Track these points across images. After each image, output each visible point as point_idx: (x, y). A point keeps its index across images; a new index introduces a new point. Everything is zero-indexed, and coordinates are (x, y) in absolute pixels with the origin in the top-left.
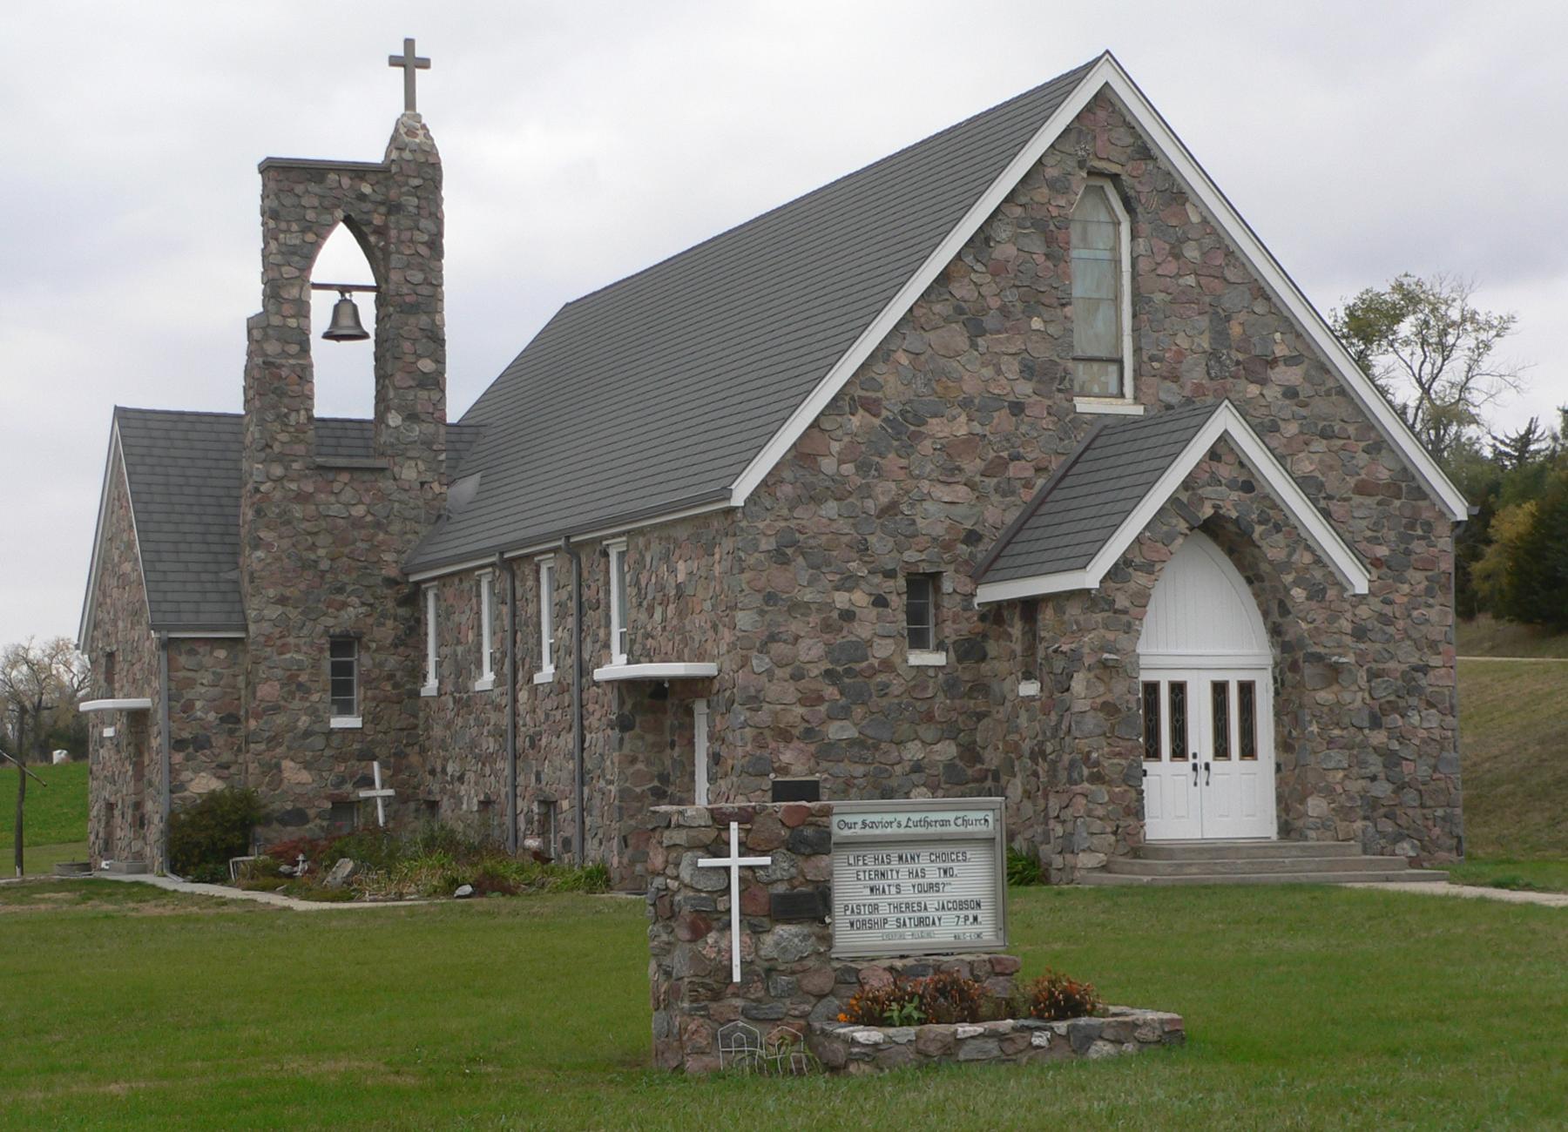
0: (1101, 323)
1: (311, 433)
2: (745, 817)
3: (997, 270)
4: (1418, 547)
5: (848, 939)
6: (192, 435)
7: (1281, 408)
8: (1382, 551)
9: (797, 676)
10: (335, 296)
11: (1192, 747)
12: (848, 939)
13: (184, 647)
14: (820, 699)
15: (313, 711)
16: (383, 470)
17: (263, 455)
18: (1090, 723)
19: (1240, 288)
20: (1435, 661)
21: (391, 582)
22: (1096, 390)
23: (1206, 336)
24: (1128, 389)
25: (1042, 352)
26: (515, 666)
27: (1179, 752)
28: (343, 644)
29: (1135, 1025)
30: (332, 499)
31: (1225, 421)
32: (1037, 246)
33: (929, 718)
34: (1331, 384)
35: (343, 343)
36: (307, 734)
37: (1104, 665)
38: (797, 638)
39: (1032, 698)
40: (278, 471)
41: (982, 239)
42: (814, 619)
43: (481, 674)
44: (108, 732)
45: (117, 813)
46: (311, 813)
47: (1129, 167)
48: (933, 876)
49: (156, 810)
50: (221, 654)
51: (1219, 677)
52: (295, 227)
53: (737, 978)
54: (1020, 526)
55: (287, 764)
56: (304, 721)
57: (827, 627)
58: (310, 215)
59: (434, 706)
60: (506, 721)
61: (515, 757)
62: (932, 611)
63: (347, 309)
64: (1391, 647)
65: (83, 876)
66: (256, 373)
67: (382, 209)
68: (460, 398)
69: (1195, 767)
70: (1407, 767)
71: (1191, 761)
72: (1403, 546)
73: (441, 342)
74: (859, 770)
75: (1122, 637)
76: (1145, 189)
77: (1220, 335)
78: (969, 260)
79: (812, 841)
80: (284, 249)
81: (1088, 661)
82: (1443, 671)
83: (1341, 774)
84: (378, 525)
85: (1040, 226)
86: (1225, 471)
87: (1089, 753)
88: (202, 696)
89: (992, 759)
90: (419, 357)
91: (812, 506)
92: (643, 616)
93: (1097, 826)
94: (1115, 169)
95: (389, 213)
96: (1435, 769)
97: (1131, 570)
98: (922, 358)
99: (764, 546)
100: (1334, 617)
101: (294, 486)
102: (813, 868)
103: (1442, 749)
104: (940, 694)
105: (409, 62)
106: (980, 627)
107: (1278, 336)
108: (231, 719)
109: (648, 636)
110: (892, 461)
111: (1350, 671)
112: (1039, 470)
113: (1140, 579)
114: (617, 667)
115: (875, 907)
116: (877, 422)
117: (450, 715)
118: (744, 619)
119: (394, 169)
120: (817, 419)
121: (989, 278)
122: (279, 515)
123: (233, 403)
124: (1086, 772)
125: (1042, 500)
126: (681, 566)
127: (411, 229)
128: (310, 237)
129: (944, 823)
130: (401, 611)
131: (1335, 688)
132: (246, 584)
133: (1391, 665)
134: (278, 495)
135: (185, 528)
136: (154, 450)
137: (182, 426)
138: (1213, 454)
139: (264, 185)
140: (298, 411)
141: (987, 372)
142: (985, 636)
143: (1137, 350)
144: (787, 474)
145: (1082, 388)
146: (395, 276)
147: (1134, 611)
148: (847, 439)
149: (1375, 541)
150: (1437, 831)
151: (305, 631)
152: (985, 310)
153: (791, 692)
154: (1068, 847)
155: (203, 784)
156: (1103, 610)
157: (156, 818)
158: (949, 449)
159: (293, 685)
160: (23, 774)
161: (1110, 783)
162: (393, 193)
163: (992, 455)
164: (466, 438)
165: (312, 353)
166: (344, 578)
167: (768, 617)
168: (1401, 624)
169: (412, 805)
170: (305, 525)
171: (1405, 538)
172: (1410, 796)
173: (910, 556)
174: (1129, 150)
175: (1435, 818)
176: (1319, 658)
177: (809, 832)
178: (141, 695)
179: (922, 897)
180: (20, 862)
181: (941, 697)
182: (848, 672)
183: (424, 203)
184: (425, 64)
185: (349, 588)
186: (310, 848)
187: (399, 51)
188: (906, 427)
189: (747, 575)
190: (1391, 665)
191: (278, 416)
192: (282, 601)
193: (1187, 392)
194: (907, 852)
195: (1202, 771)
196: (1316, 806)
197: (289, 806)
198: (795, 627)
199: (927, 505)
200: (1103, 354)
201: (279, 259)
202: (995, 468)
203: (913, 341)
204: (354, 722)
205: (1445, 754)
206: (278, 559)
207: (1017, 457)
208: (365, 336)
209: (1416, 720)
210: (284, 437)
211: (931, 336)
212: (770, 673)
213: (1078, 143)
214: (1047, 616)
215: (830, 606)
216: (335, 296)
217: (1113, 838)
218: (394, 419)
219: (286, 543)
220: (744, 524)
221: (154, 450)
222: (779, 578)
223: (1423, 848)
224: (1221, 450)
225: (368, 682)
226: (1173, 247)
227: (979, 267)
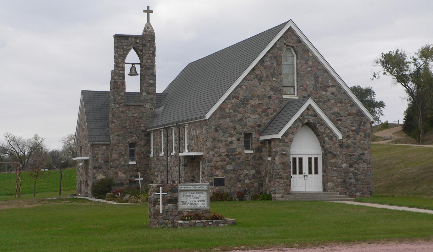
0: (290, 79)
1: (125, 97)
2: (163, 186)
3: (265, 68)
4: (362, 127)
5: (181, 206)
6: (99, 97)
8: (354, 128)
9: (220, 156)
10: (131, 66)
11: (303, 172)
12: (181, 206)
13: (96, 146)
14: (225, 161)
15: (125, 160)
16: (141, 105)
17: (114, 102)
18: (279, 166)
20: (366, 152)
21: (143, 131)
22: (288, 93)
23: (313, 81)
24: (296, 93)
25: (275, 85)
26: (168, 151)
27: (301, 172)
28: (132, 145)
29: (227, 221)
30: (130, 112)
31: (310, 102)
32: (275, 63)
33: (249, 164)
34: (342, 91)
36: (124, 166)
37: (282, 154)
38: (220, 148)
39: (270, 161)
40: (117, 106)
41: (262, 61)
42: (224, 143)
43: (161, 153)
44: (80, 164)
45: (82, 183)
46: (125, 183)
47: (296, 44)
48: (197, 196)
49: (90, 182)
50: (105, 147)
51: (310, 156)
53: (161, 212)
54: (270, 123)
55: (119, 172)
56: (123, 163)
57: (227, 145)
58: (125, 47)
59: (152, 159)
60: (166, 164)
61: (167, 171)
62: (250, 141)
63: (133, 69)
65: (74, 197)
66: (112, 84)
68: (160, 89)
69: (304, 176)
70: (359, 176)
71: (303, 174)
73: (155, 76)
74: (233, 176)
75: (286, 148)
76: (300, 49)
77: (316, 81)
78: (259, 65)
79: (174, 190)
82: (368, 155)
83: (336, 178)
84: (140, 118)
85: (275, 58)
86: (310, 112)
88: (100, 157)
89: (263, 173)
90: (150, 79)
92: (191, 142)
93: (280, 188)
94: (293, 45)
95: (143, 47)
96: (365, 176)
99: (213, 128)
100: (335, 144)
101: (121, 109)
102: (175, 195)
103: (367, 172)
104: (252, 160)
105: (148, 11)
106: (261, 145)
107: (330, 81)
108: (107, 162)
109: (191, 146)
110: (241, 109)
112: (274, 111)
113: (291, 136)
114: (186, 153)
115: (187, 201)
116: (238, 101)
117: (155, 162)
118: (208, 143)
119: (144, 36)
120: (225, 101)
122: (118, 116)
124: (278, 177)
125: (275, 117)
126: (197, 131)
128: (125, 52)
129: (199, 187)
130: (145, 138)
131: (335, 159)
132: (110, 131)
133: (356, 153)
134: (117, 111)
135: (97, 118)
136: (89, 99)
137: (97, 94)
138: (308, 109)
139: (115, 41)
141: (263, 90)
142: (262, 147)
143: (297, 85)
146: (144, 61)
147: (290, 143)
148: (231, 105)
149: (352, 126)
150: (366, 190)
151: (123, 142)
152: (262, 76)
153: (218, 159)
154: (275, 193)
155: (100, 177)
157: (90, 184)
158: (254, 106)
159: (121, 154)
160: (61, 174)
161: (284, 179)
162: (144, 42)
163: (264, 108)
164: (163, 97)
165: (125, 79)
166: (132, 130)
168: (358, 144)
169: (148, 182)
170: (124, 118)
172: (359, 182)
173: (245, 130)
176: (331, 153)
177: (174, 189)
178: (87, 156)
179: (195, 200)
180: (60, 194)
181: (252, 160)
184: (152, 12)
185: (134, 132)
186: (122, 191)
187: (146, 9)
188: (244, 102)
189: (209, 134)
190: (356, 153)
191: (117, 93)
192: (118, 135)
193: (309, 94)
194: (192, 192)
196: (330, 184)
197: (120, 182)
198: (219, 145)
199: (249, 119)
200: (290, 85)
201: (118, 57)
202: (265, 111)
203: (246, 83)
204: (134, 163)
206: (117, 126)
207: (269, 108)
208: (138, 75)
209: (361, 165)
211: (250, 82)
212: (214, 155)
214: (273, 143)
215: (227, 141)
216: (131, 66)
218: (144, 94)
219: (119, 122)
221: (89, 99)
222: (216, 135)
223: (362, 194)
224: (309, 108)
225: (138, 154)
226: (306, 62)
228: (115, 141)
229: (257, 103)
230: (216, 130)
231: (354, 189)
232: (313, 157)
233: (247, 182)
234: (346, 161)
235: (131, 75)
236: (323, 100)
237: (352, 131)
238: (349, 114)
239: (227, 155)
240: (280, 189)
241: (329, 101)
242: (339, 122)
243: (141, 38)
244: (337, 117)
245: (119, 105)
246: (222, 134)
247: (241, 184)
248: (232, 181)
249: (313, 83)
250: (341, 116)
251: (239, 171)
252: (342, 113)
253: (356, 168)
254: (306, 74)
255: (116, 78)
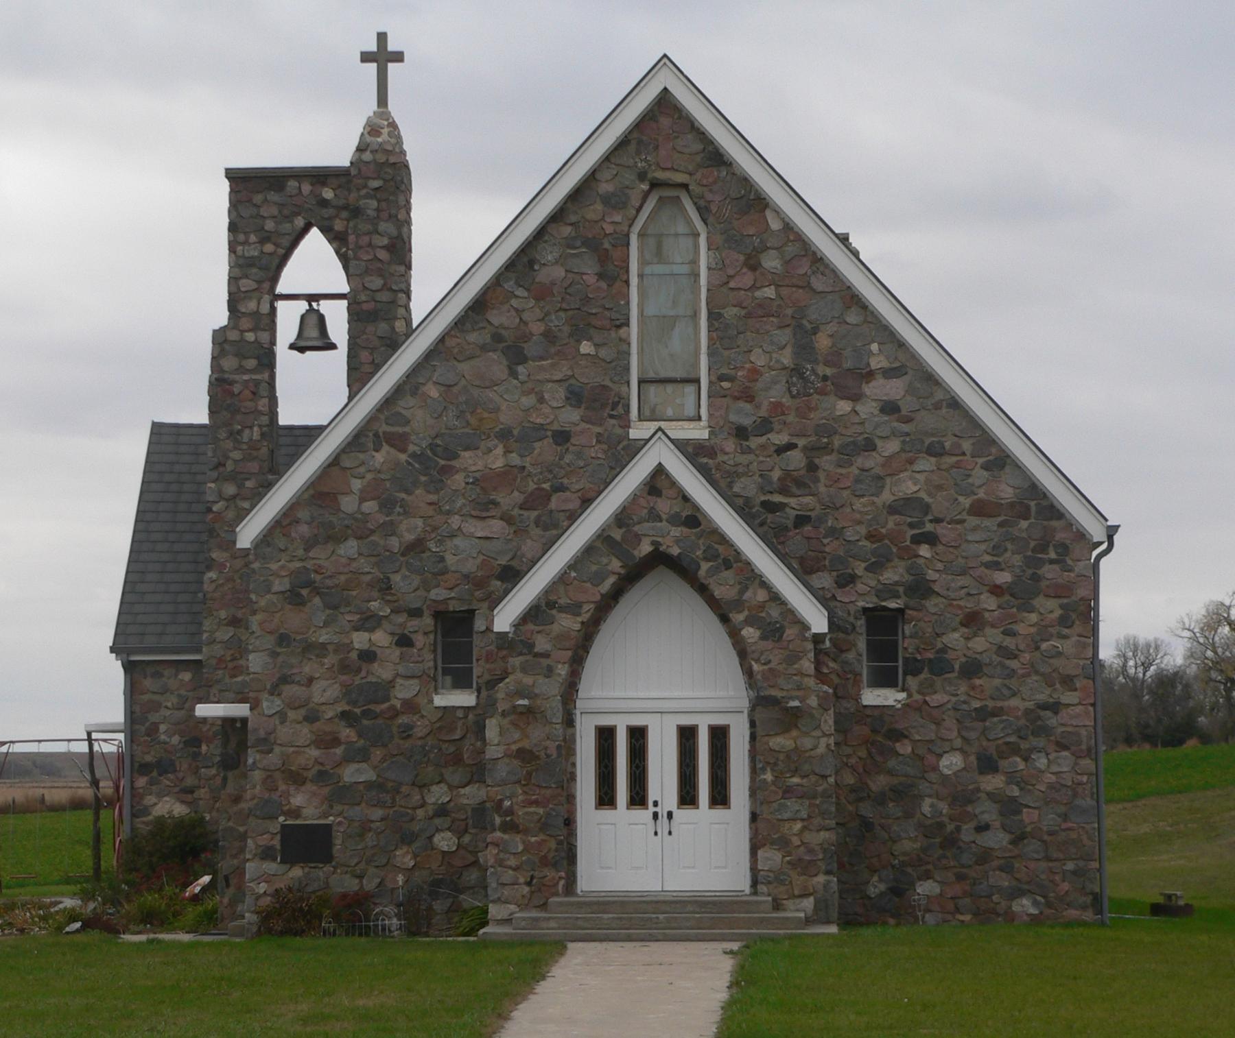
0: (676, 343)
7: (877, 426)
8: (1003, 578)
9: (312, 718)
10: (303, 306)
11: (652, 795)
14: (335, 741)
17: (215, 474)
19: (830, 297)
20: (1068, 697)
22: (670, 412)
23: (788, 351)
27: (638, 798)
32: (588, 268)
34: (939, 395)
35: (308, 353)
38: (311, 680)
40: (230, 489)
47: (698, 176)
50: (186, 676)
51: (687, 721)
52: (253, 238)
57: (344, 667)
58: (270, 225)
63: (313, 320)
64: (1013, 683)
67: (345, 214)
71: (652, 809)
72: (1030, 572)
74: (378, 813)
75: (541, 680)
76: (718, 198)
77: (804, 349)
80: (241, 261)
81: (502, 706)
82: (1079, 709)
85: (593, 245)
86: (664, 506)
87: (501, 801)
91: (330, 547)
94: (680, 178)
96: (1065, 817)
97: (554, 612)
98: (455, 390)
99: (277, 587)
100: (793, 658)
103: (1075, 795)
107: (875, 347)
110: (420, 498)
111: (812, 716)
116: (403, 457)
119: (353, 172)
121: (532, 302)
123: (200, 416)
127: (369, 233)
131: (794, 733)
140: (251, 428)
144: (303, 514)
145: (653, 411)
148: (369, 476)
149: (996, 566)
152: (527, 337)
153: (305, 733)
155: (169, 807)
156: (521, 654)
158: (484, 483)
161: (526, 832)
163: (532, 486)
167: (280, 659)
171: (1033, 562)
172: (1032, 847)
174: (698, 158)
175: (1064, 872)
182: (366, 714)
183: (384, 204)
184: (398, 57)
187: (372, 47)
188: (435, 462)
190: (1014, 702)
191: (231, 434)
193: (763, 413)
195: (663, 819)
199: (457, 541)
200: (679, 374)
205: (1079, 802)
207: (560, 488)
208: (332, 347)
209: (1042, 762)
210: (236, 455)
211: (464, 367)
212: (282, 716)
213: (638, 153)
215: (349, 647)
216: (303, 306)
217: (526, 889)
220: (256, 565)
222: (293, 620)
223: (1049, 905)
226: (749, 257)
227: (520, 292)
228: (218, 650)
229: (499, 464)
230: (294, 598)
231: (1005, 882)
232: (622, 727)
233: (445, 841)
234: (958, 743)
235: (302, 350)
236: (837, 442)
237: (996, 590)
238: (979, 509)
239: (344, 715)
240: (504, 880)
241: (870, 446)
242: (924, 551)
243: (343, 180)
244: (911, 526)
245: (240, 486)
246: (320, 618)
247: (415, 856)
248: (370, 839)
249: (786, 358)
250: (937, 521)
251: (404, 789)
252: (939, 503)
253: (1012, 778)
254: (749, 316)
255: (229, 363)
